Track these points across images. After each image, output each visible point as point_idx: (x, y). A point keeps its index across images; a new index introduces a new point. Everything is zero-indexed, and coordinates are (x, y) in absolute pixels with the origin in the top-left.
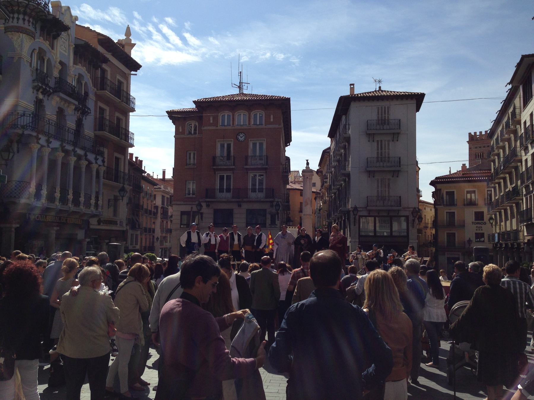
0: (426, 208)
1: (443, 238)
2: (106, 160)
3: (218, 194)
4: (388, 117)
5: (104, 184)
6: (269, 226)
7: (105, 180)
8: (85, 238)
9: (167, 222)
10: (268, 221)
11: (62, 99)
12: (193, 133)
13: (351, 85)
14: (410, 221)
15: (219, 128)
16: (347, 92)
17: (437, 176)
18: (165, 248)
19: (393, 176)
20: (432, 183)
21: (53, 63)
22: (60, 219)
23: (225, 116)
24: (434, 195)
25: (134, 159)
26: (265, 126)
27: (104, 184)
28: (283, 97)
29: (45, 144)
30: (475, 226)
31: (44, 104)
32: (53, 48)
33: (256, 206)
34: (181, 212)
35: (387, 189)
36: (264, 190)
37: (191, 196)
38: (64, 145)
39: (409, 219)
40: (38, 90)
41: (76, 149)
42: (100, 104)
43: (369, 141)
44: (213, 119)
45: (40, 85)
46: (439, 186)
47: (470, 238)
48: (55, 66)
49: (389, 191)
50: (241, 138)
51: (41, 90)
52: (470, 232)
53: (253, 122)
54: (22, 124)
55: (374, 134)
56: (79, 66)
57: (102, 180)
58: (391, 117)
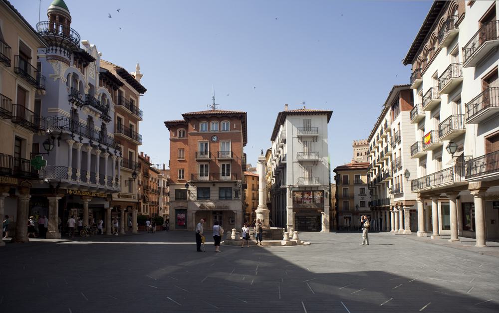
2: (122, 153)
8: (110, 207)
11: (91, 110)
20: (335, 171)
22: (91, 194)
23: (203, 126)
25: (144, 156)
29: (78, 140)
30: (360, 197)
31: (78, 113)
40: (73, 103)
41: (101, 145)
42: (118, 115)
45: (74, 99)
46: (339, 172)
48: (85, 86)
51: (75, 103)
56: (103, 88)
57: (120, 167)
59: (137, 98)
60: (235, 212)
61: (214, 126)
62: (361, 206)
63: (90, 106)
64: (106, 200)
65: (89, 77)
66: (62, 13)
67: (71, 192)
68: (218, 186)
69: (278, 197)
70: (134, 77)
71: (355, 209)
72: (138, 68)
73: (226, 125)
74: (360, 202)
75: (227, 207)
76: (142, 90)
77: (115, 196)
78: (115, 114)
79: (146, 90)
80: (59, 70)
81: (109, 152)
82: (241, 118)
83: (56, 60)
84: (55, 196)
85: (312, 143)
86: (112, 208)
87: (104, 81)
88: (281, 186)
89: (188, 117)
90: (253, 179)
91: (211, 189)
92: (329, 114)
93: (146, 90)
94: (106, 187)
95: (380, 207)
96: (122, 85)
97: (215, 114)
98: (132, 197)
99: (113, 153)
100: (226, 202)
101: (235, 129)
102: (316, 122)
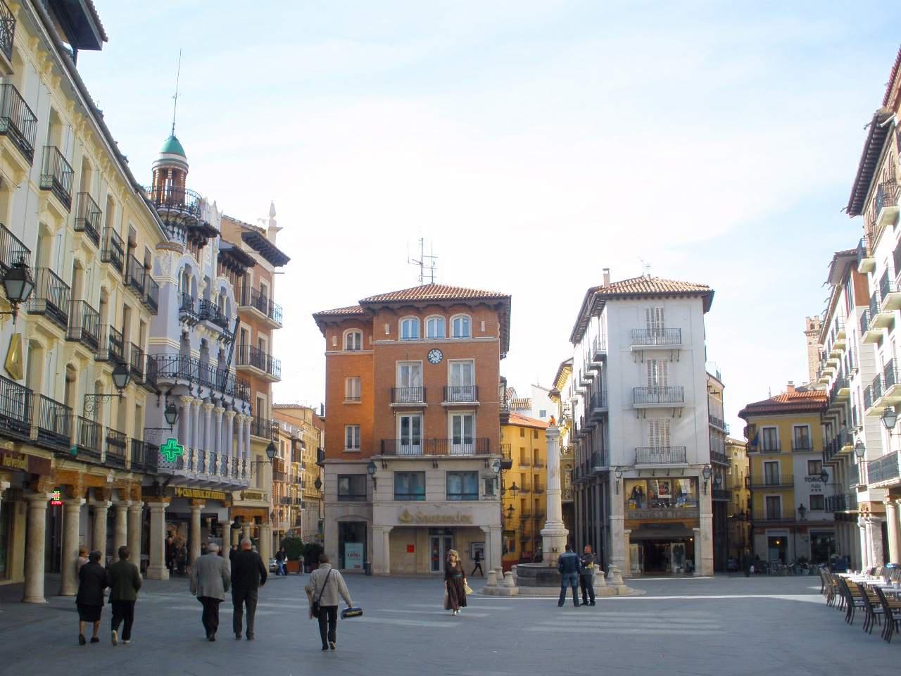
0: (738, 453)
1: (761, 506)
3: (401, 450)
4: (663, 324)
5: (252, 442)
6: (483, 498)
7: (254, 436)
8: (229, 520)
9: (282, 486)
10: (482, 490)
11: (207, 328)
12: (354, 347)
13: (605, 270)
14: (700, 485)
15: (400, 341)
16: (598, 282)
17: (749, 403)
18: (280, 531)
19: (673, 416)
20: (742, 415)
21: (198, 280)
23: (407, 326)
24: (748, 431)
26: (473, 338)
27: (252, 442)
28: (495, 294)
30: (808, 484)
31: (189, 338)
32: (198, 261)
33: (462, 467)
34: (339, 475)
35: (665, 436)
36: (474, 442)
37: (354, 449)
38: (214, 392)
39: (700, 482)
41: (225, 396)
43: (638, 417)
44: (390, 328)
46: (753, 419)
47: (802, 505)
48: (200, 285)
49: (668, 439)
50: (436, 357)
52: (802, 494)
53: (453, 332)
54: (175, 372)
55: (645, 409)
57: (249, 436)
58: (667, 325)
59: (269, 277)
60: (485, 529)
61: (433, 326)
62: (812, 509)
63: (208, 323)
64: (221, 504)
65: (266, 314)
66: (175, 165)
67: (180, 492)
68: (444, 467)
69: (589, 489)
70: (264, 232)
71: (798, 517)
72: (273, 214)
73: (460, 325)
74: (811, 496)
75: (466, 518)
76: (278, 259)
77: (236, 495)
78: (238, 321)
79: (289, 259)
80: (169, 266)
81: (234, 409)
82: (497, 307)
83: (166, 249)
84: (160, 501)
85: (668, 365)
86: (232, 522)
87: (224, 265)
88: (598, 468)
89: (371, 306)
90: (522, 435)
91: (427, 475)
92: (706, 297)
93: (289, 259)
94: (219, 478)
95: (841, 514)
96: (252, 263)
97: (437, 300)
98: (263, 496)
99: (240, 410)
100: (463, 506)
101: (485, 334)
102: (676, 316)
